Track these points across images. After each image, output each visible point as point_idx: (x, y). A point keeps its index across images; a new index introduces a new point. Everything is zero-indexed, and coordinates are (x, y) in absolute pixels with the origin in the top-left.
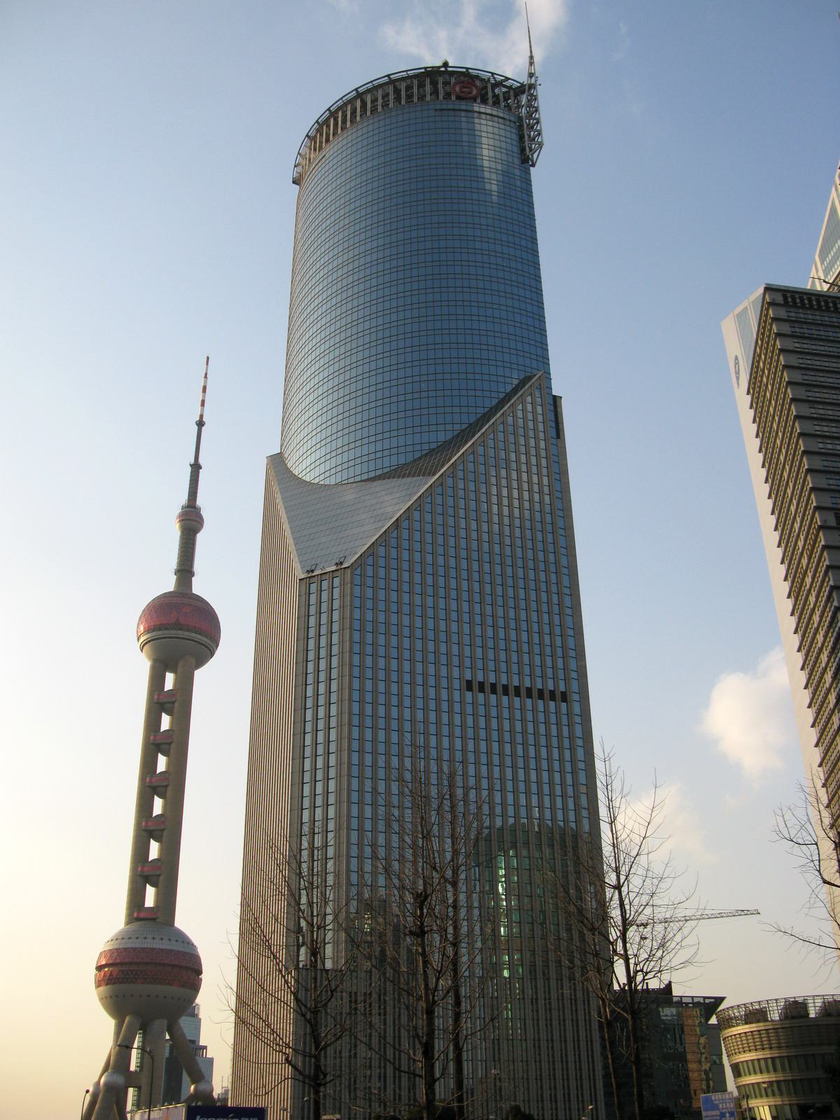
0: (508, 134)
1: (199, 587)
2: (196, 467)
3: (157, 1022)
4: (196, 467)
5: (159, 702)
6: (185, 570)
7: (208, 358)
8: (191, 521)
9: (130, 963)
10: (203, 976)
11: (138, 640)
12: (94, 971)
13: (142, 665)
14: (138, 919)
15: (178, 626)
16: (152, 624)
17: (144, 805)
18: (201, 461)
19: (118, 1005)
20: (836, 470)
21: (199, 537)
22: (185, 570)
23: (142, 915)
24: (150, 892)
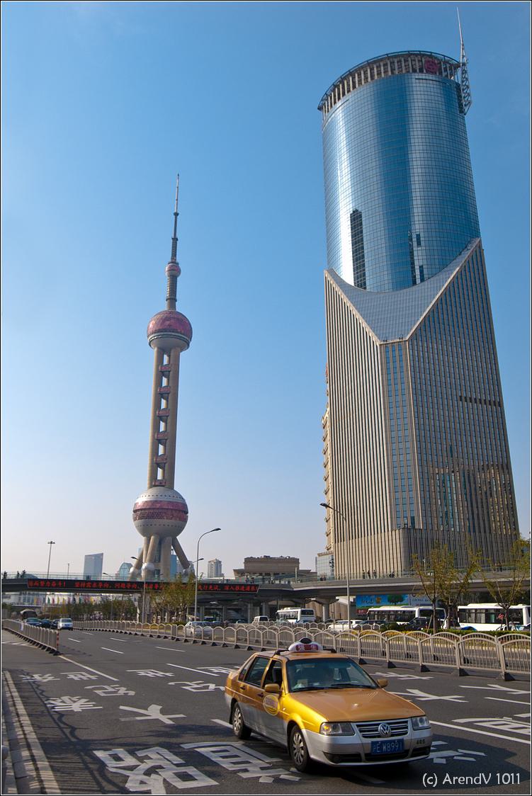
0: (439, 91)
1: (179, 308)
2: (175, 240)
3: (167, 538)
4: (175, 240)
5: (161, 372)
6: (172, 299)
7: (219, 529)
8: (174, 273)
9: (149, 509)
10: (189, 515)
11: (148, 337)
12: (133, 513)
13: (153, 352)
14: (155, 486)
15: (173, 270)
16: (157, 328)
17: (157, 404)
18: (178, 236)
19: (145, 531)
20: (418, 281)
21: (179, 279)
22: (172, 299)
23: (157, 484)
24: (161, 448)
